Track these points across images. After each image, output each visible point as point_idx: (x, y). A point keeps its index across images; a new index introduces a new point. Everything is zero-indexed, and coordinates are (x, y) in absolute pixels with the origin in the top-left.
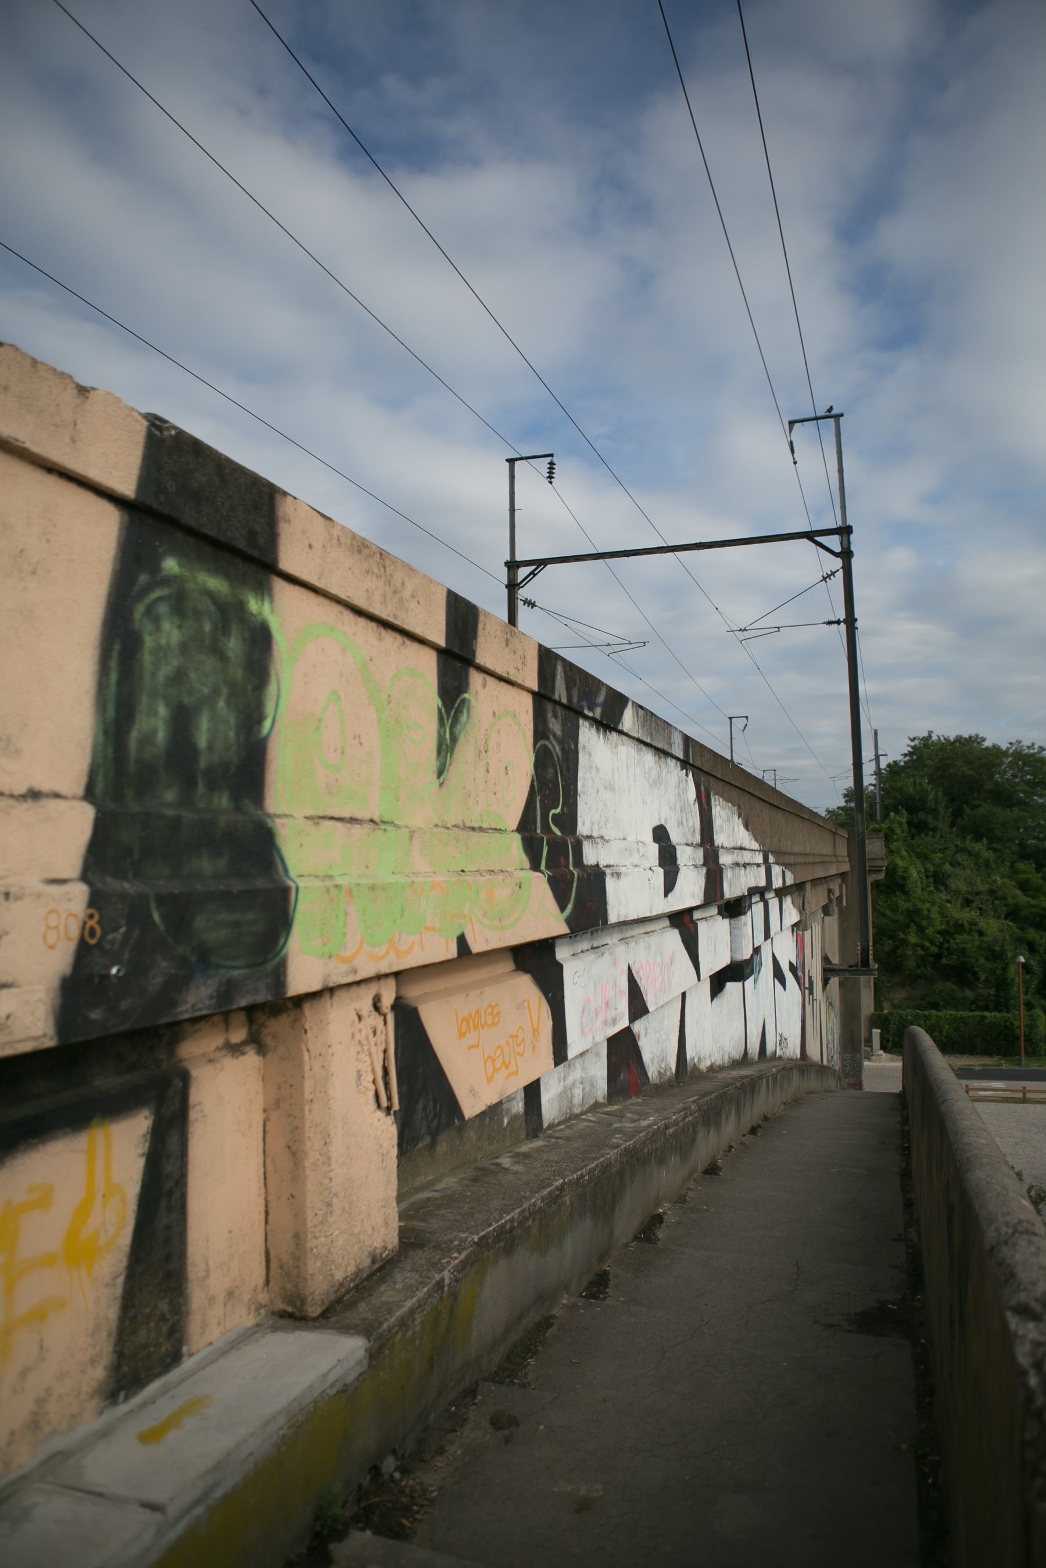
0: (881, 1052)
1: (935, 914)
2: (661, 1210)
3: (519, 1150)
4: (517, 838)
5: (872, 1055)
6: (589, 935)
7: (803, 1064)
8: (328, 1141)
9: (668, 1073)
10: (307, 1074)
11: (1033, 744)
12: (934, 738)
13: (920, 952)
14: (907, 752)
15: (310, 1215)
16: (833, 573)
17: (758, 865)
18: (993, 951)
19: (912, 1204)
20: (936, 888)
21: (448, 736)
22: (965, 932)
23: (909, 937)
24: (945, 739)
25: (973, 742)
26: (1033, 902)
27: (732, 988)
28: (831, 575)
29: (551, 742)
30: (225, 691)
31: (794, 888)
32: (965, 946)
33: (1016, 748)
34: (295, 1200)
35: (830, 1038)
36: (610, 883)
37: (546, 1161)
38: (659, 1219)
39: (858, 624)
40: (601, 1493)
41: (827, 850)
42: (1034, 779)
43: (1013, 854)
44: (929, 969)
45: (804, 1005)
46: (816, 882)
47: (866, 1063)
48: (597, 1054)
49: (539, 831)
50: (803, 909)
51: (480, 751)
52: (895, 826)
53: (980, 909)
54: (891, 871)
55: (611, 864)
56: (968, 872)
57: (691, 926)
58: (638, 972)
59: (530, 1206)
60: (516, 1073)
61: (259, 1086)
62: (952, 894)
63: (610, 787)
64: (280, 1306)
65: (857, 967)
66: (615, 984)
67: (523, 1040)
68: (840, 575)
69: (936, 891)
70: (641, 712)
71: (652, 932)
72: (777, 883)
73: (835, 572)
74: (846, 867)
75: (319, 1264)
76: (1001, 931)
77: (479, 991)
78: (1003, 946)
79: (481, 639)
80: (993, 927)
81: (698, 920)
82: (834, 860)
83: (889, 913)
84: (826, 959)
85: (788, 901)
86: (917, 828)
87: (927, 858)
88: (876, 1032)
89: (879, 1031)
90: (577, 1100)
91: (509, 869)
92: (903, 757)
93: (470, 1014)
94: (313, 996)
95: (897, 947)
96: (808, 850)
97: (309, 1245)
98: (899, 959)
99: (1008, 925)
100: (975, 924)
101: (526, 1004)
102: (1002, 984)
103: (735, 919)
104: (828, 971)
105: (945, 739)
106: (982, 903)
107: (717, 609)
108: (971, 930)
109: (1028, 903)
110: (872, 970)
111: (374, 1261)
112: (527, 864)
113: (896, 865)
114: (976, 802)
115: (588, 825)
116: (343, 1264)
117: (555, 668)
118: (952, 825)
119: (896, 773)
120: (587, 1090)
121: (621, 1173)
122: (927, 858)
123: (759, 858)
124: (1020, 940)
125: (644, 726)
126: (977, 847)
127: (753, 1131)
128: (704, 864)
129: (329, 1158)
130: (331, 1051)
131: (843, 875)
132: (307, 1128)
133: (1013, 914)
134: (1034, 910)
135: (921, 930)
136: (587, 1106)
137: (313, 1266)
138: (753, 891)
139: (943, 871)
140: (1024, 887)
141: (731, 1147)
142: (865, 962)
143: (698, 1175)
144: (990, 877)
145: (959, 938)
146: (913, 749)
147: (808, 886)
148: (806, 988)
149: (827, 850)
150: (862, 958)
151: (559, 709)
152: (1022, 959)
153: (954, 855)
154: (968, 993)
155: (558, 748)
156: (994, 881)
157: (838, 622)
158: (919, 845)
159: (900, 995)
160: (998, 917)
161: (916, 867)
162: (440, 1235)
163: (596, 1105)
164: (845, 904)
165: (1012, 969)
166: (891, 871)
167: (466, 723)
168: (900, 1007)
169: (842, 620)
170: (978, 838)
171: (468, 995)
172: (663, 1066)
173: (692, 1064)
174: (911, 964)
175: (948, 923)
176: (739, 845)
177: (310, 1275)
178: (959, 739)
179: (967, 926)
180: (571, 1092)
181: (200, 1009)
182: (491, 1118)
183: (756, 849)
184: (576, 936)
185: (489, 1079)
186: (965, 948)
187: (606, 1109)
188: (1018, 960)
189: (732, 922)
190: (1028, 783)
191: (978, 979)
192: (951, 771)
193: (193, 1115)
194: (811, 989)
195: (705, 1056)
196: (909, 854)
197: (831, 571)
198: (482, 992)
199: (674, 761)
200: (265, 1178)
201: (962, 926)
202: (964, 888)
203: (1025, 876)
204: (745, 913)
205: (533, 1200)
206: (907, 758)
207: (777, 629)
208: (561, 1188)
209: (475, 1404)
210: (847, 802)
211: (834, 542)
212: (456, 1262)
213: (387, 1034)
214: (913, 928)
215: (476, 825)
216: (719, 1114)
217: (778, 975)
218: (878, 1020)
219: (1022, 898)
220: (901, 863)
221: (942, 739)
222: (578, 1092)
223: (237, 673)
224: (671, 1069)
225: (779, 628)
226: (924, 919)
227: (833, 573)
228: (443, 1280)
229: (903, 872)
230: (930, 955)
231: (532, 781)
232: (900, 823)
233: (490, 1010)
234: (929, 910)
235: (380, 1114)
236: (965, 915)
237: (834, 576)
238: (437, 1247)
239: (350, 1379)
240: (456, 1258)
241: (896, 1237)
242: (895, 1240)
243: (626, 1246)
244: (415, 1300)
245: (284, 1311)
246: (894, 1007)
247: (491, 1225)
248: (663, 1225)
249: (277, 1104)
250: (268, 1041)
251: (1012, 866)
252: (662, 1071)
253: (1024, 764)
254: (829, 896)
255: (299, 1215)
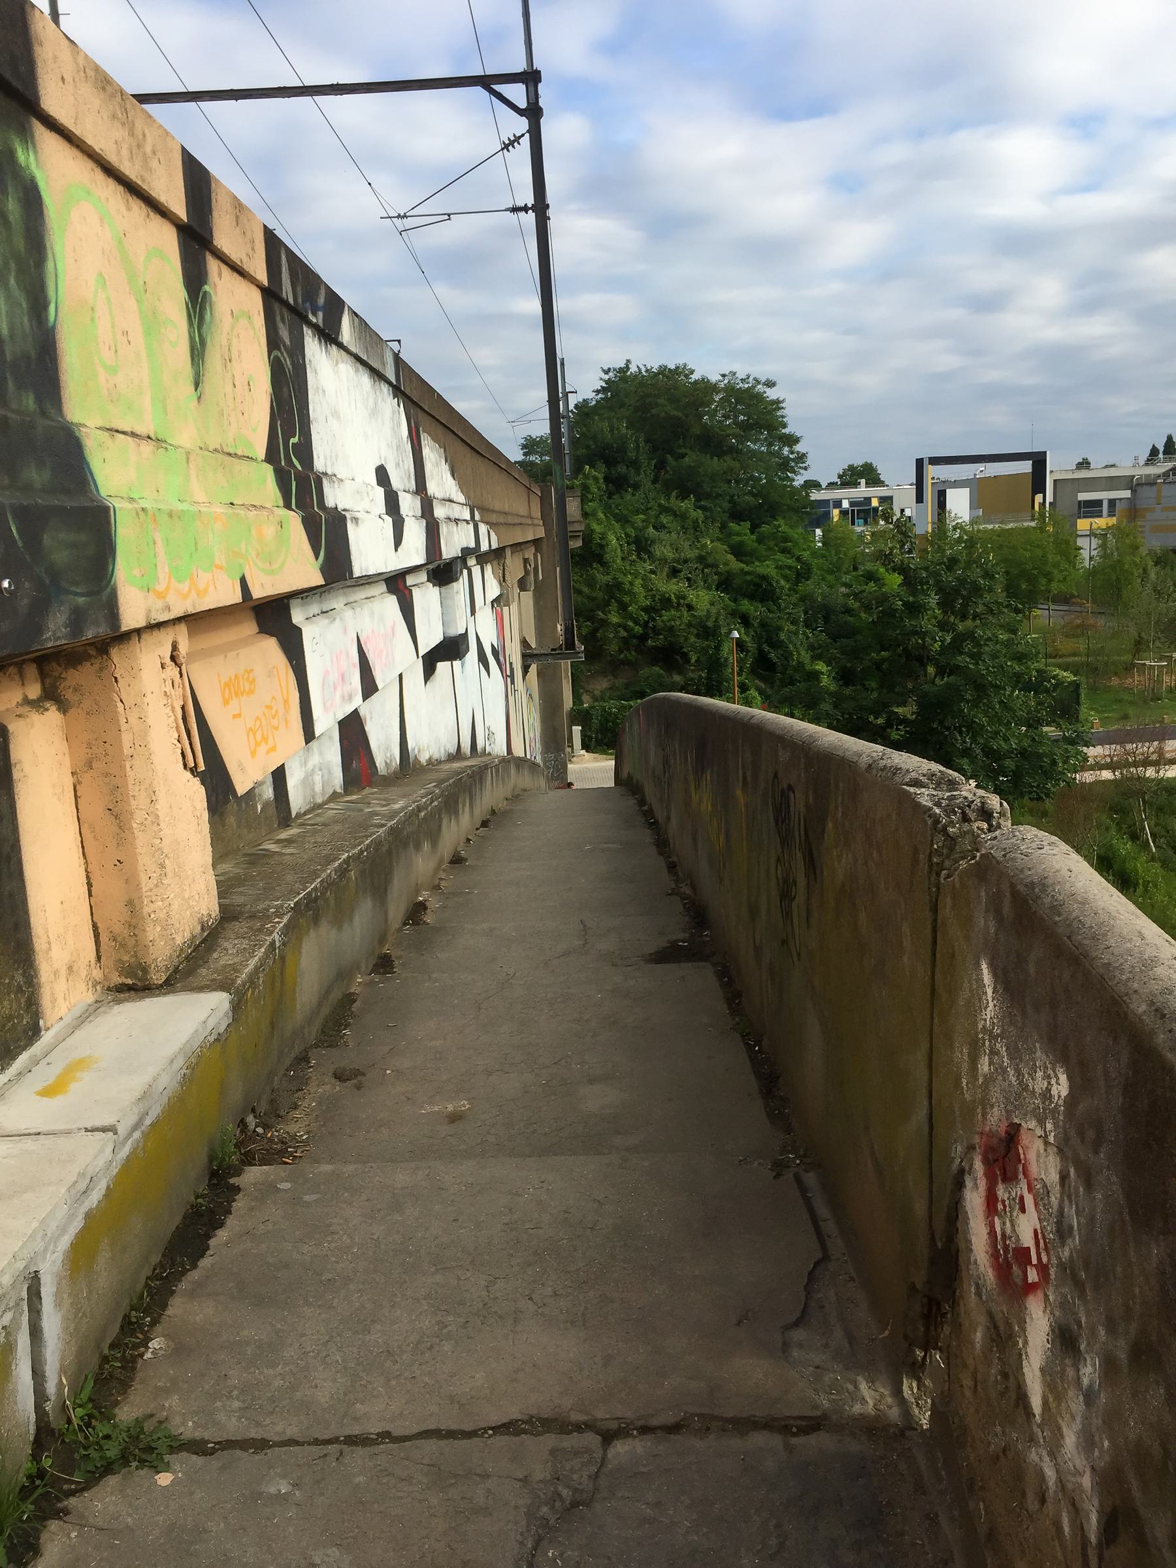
0: (583, 752)
1: (638, 588)
2: (421, 899)
3: (278, 837)
4: (268, 471)
5: (573, 756)
6: (317, 596)
7: (510, 761)
8: (154, 799)
9: (394, 764)
10: (124, 727)
11: (748, 377)
12: (633, 369)
13: (623, 634)
14: (600, 388)
15: (143, 878)
16: (517, 139)
17: (467, 522)
18: (705, 627)
19: (675, 866)
20: (639, 557)
21: (197, 339)
22: (673, 607)
23: (609, 616)
24: (647, 371)
25: (679, 374)
26: (747, 568)
27: (442, 667)
28: (514, 141)
29: (282, 354)
30: (13, 265)
31: (493, 555)
32: (673, 623)
33: (729, 382)
34: (124, 866)
35: (532, 736)
36: (350, 527)
37: (315, 843)
38: (422, 906)
39: (550, 212)
40: (467, 1106)
41: (523, 511)
42: (748, 420)
43: (724, 512)
44: (633, 653)
45: (507, 696)
46: (517, 547)
47: (570, 766)
48: (331, 738)
49: (283, 463)
50: (504, 581)
51: (226, 360)
52: (590, 482)
53: (689, 579)
54: (588, 537)
55: (347, 508)
56: (674, 535)
57: (406, 592)
58: (365, 643)
59: (328, 876)
60: (274, 749)
61: (64, 747)
62: (657, 563)
63: (336, 414)
64: (117, 979)
65: (561, 650)
66: (348, 656)
67: (277, 711)
68: (526, 141)
69: (639, 560)
70: (356, 319)
71: (373, 597)
72: (484, 547)
73: (520, 137)
74: (541, 533)
75: (158, 929)
76: (712, 604)
77: (235, 653)
78: (716, 621)
79: (215, 214)
80: (703, 599)
81: (411, 586)
82: (530, 522)
83: (586, 589)
84: (524, 643)
85: (488, 569)
86: (616, 484)
87: (627, 521)
88: (577, 729)
89: (580, 728)
90: (318, 788)
91: (269, 506)
92: (594, 394)
93: (230, 678)
94: (138, 632)
95: (596, 630)
96: (507, 510)
97: (146, 910)
98: (599, 644)
99: (720, 597)
100: (684, 598)
101: (275, 670)
102: (715, 665)
103: (446, 587)
104: (528, 657)
105: (647, 371)
106: (690, 573)
107: (370, 184)
108: (679, 604)
109: (742, 570)
110: (579, 653)
111: (203, 929)
112: (281, 503)
113: (592, 531)
114: (683, 451)
115: (322, 460)
116: (181, 929)
117: (279, 253)
118: (655, 481)
119: (587, 415)
120: (326, 778)
121: (389, 852)
122: (627, 521)
123: (467, 515)
124: (733, 614)
125: (360, 338)
126: (686, 505)
127: (485, 824)
128: (422, 517)
129: (157, 817)
130: (146, 700)
131: (536, 542)
132: (130, 786)
133: (725, 584)
134: (748, 578)
135: (623, 607)
136: (327, 796)
137: (153, 932)
138: (466, 552)
139: (646, 536)
140: (738, 551)
141: (468, 840)
142: (570, 644)
143: (445, 865)
144: (698, 542)
145: (666, 615)
146: (606, 384)
147: (508, 552)
148: (509, 677)
149: (523, 511)
150: (566, 639)
151: (285, 311)
152: (736, 634)
153: (657, 517)
154: (677, 678)
155: (288, 363)
156: (705, 545)
157: (525, 209)
158: (617, 506)
159: (601, 685)
160: (709, 588)
161: (615, 532)
162: (251, 906)
163: (334, 796)
164: (541, 578)
165: (726, 649)
166: (588, 537)
167: (211, 323)
168: (603, 699)
169: (530, 205)
170: (683, 496)
171: (226, 656)
172: (388, 755)
173: (413, 755)
174: (613, 648)
175: (653, 596)
176: (447, 496)
177: (151, 941)
178: (663, 370)
179: (675, 600)
180: (312, 779)
181: (59, 638)
182: (247, 803)
183: (462, 502)
184: (307, 596)
185: (253, 754)
186: (673, 627)
187: (346, 799)
188: (732, 636)
189: (443, 589)
190: (740, 425)
191: (688, 661)
192: (654, 411)
193: (16, 774)
194: (512, 676)
195: (424, 747)
196: (606, 516)
197: (514, 135)
198: (237, 654)
199: (387, 386)
200: (83, 847)
201: (669, 600)
202: (670, 555)
203: (739, 538)
204: (457, 580)
205: (329, 871)
206: (600, 396)
207: (447, 217)
208: (347, 861)
209: (311, 1067)
210: (525, 454)
211: (517, 93)
212: (281, 925)
213: (183, 685)
214: (614, 605)
215: (232, 451)
216: (457, 802)
217: (482, 659)
218: (580, 716)
219: (735, 565)
220: (595, 526)
221: (643, 370)
222: (318, 779)
223: (20, 244)
224: (395, 759)
225: (449, 215)
226: (626, 594)
227: (517, 139)
228: (274, 941)
229: (601, 539)
230: (634, 636)
231: (272, 402)
232: (596, 479)
233: (246, 676)
234: (631, 584)
235: (188, 774)
236: (672, 588)
237: (519, 143)
238: (253, 916)
239: (222, 1029)
240: (279, 923)
241: (670, 892)
242: (669, 894)
243: (400, 930)
244: (256, 959)
245: (123, 984)
246: (595, 699)
247: (300, 894)
248: (428, 911)
249: (89, 765)
250: (69, 695)
251: (723, 527)
252: (388, 761)
253: (737, 402)
254: (525, 567)
255: (131, 880)
